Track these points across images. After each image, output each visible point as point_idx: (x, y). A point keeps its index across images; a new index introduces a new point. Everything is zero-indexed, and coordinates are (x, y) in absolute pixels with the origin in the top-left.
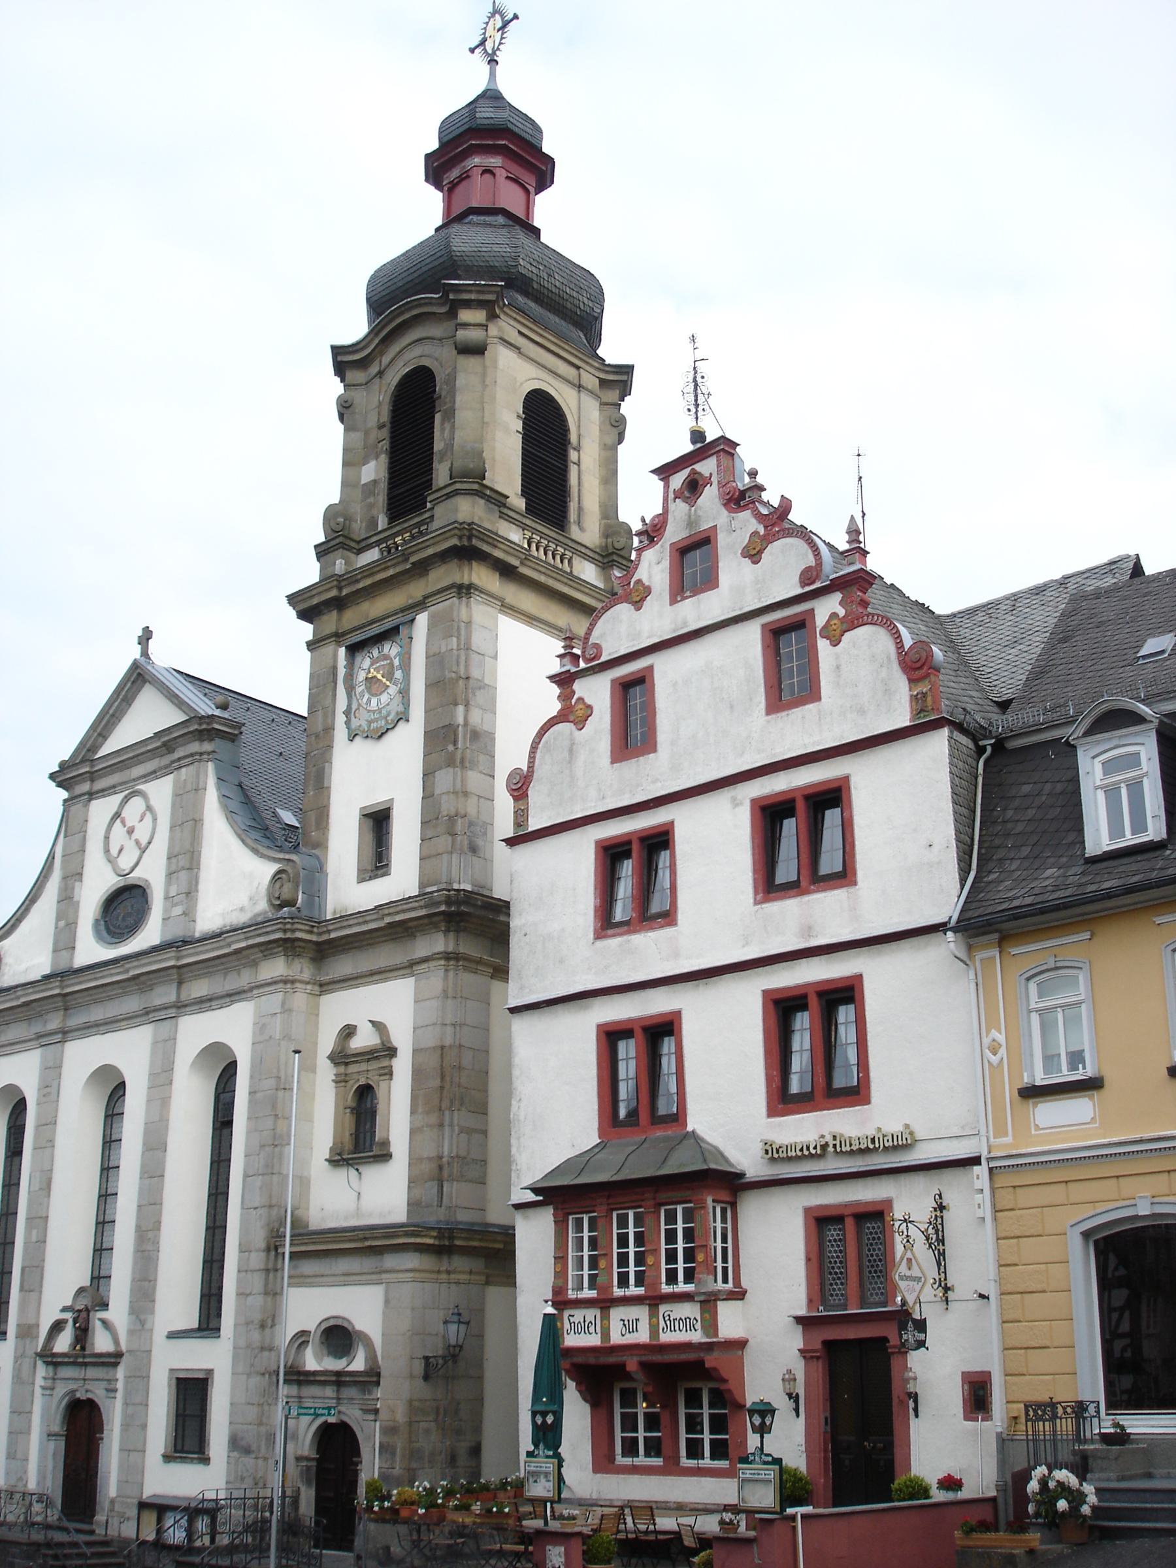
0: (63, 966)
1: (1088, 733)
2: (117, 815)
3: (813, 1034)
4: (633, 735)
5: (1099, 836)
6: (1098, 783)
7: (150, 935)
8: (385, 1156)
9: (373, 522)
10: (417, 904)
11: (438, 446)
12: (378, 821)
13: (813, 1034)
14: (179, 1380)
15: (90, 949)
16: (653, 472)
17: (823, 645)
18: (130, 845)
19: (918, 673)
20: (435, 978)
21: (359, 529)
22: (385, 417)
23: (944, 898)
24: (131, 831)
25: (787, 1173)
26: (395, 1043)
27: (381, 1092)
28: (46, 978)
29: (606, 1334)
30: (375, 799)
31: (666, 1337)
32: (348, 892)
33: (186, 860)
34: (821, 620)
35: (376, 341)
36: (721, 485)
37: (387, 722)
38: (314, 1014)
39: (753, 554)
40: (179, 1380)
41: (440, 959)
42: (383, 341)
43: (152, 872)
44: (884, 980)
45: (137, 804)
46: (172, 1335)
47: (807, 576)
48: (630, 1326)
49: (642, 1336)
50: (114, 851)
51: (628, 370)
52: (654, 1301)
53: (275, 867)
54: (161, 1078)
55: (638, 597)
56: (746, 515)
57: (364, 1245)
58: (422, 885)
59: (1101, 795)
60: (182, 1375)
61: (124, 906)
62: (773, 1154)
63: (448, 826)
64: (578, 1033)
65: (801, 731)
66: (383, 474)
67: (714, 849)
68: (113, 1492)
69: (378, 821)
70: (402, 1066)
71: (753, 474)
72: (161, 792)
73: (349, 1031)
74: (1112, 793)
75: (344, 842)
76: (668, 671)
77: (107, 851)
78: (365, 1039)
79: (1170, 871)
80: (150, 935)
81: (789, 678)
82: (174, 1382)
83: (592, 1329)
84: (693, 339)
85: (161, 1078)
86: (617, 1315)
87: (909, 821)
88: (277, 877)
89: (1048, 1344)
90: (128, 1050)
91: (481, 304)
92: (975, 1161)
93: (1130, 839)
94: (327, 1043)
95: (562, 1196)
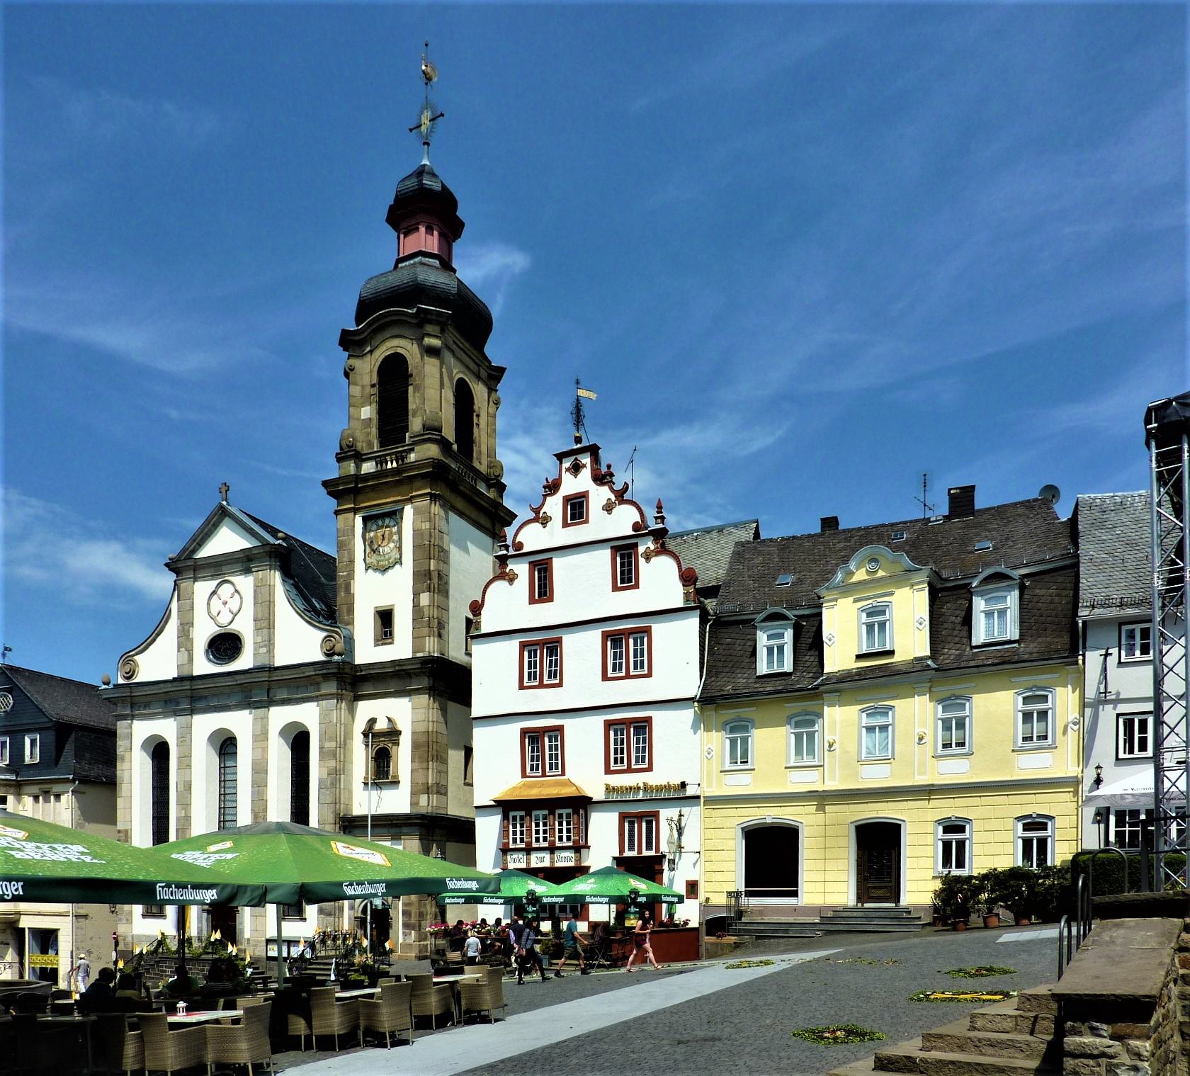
0: (185, 673)
1: (763, 621)
2: (214, 593)
3: (630, 734)
4: (542, 591)
5: (763, 668)
7: (245, 661)
8: (396, 783)
9: (370, 444)
11: (411, 406)
12: (385, 618)
13: (630, 734)
15: (203, 666)
17: (642, 561)
18: (225, 611)
20: (424, 699)
21: (361, 446)
22: (375, 380)
23: (691, 685)
24: (225, 603)
26: (399, 727)
27: (393, 753)
28: (175, 680)
29: (528, 863)
30: (384, 603)
31: (558, 865)
32: (367, 652)
33: (265, 622)
34: (641, 549)
36: (593, 470)
38: (352, 711)
39: (608, 508)
43: (244, 627)
44: (660, 718)
45: (226, 590)
47: (636, 527)
49: (547, 864)
50: (214, 613)
51: (501, 370)
52: (552, 849)
53: (325, 634)
54: (261, 737)
55: (545, 521)
56: (606, 488)
57: (390, 825)
58: (414, 652)
61: (225, 645)
62: (609, 789)
63: (431, 622)
64: (512, 731)
65: (628, 602)
66: (375, 417)
67: (582, 652)
68: (247, 934)
69: (385, 618)
70: (405, 742)
71: (609, 467)
72: (245, 583)
73: (372, 721)
74: (770, 650)
75: (363, 626)
76: (559, 565)
77: (209, 611)
78: (381, 725)
80: (245, 661)
81: (626, 577)
85: (261, 737)
86: (534, 856)
87: (678, 654)
88: (326, 639)
90: (239, 722)
91: (438, 323)
92: (698, 797)
93: (776, 670)
94: (359, 725)
95: (506, 807)
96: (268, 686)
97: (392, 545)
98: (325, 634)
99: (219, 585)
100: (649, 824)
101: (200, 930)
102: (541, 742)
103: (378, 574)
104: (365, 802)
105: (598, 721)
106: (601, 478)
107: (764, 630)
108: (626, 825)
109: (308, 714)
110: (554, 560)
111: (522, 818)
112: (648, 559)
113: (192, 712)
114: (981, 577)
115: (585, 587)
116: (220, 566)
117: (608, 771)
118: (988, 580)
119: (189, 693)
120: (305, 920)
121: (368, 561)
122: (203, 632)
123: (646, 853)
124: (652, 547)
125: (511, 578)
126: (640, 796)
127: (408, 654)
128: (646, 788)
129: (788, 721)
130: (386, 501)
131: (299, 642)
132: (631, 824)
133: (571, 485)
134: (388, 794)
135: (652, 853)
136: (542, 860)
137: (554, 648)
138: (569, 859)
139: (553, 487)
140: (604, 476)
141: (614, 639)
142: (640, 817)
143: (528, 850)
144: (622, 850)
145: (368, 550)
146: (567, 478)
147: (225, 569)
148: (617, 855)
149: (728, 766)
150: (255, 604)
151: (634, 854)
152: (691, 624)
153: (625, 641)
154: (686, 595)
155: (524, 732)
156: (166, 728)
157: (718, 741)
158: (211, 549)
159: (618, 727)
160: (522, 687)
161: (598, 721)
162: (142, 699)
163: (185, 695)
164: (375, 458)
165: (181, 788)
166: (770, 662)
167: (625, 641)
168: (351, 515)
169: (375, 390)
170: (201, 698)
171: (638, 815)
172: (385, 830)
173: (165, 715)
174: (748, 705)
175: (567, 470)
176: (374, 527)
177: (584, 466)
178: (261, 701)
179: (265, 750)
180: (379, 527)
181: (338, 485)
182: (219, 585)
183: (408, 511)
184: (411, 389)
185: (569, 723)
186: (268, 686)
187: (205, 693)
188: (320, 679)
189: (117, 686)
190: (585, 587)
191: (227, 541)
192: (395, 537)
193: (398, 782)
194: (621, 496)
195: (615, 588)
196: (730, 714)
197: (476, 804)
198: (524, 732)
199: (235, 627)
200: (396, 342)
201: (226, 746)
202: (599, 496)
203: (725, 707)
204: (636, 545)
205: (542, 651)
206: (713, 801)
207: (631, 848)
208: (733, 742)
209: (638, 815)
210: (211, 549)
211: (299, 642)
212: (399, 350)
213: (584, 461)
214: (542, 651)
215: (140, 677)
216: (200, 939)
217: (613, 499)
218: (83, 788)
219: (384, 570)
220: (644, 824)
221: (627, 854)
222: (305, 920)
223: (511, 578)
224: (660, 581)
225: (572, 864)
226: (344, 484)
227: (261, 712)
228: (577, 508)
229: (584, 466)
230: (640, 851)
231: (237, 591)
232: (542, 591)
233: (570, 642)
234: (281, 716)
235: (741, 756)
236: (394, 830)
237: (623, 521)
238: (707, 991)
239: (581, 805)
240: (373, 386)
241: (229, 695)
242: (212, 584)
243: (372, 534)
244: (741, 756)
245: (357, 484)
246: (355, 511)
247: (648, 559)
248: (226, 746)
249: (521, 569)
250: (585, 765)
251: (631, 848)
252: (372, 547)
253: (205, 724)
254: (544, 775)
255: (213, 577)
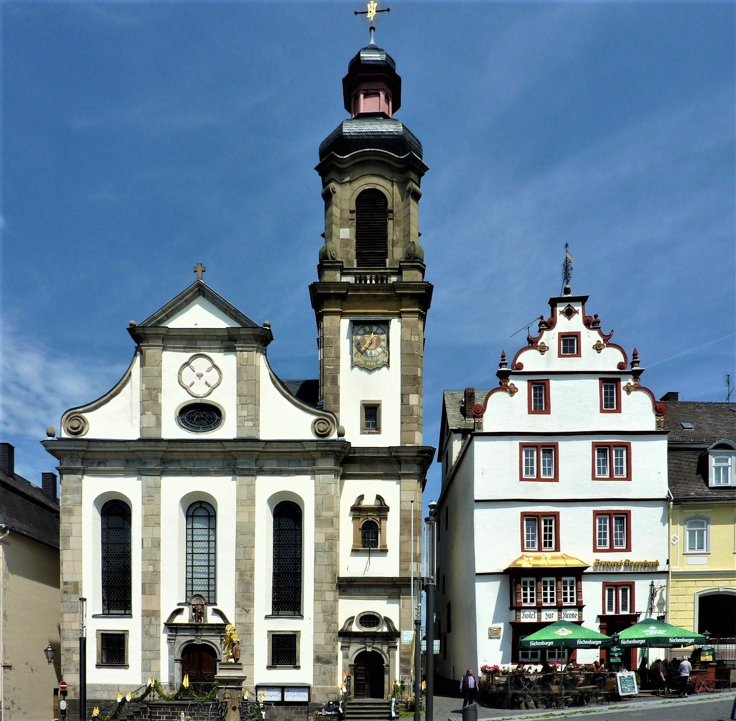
0: (152, 435)
2: (187, 364)
3: (614, 523)
4: (540, 402)
6: (713, 465)
7: (227, 430)
8: (384, 551)
10: (412, 450)
12: (371, 414)
13: (614, 523)
14: (273, 635)
15: (172, 430)
16: (588, 297)
17: (623, 393)
19: (660, 414)
23: (662, 490)
25: (602, 572)
29: (539, 618)
30: (372, 398)
33: (249, 398)
34: (623, 384)
35: (352, 163)
37: (377, 364)
39: (598, 348)
40: (102, 634)
41: (417, 475)
42: (354, 165)
43: (225, 398)
44: (638, 513)
45: (201, 364)
46: (94, 616)
47: (620, 366)
48: (551, 616)
52: (560, 608)
53: (315, 418)
54: (246, 502)
55: (543, 349)
58: (401, 443)
59: (714, 469)
60: (104, 632)
67: (576, 457)
72: (227, 362)
74: (718, 469)
76: (556, 386)
77: (220, 373)
78: (369, 501)
79: (735, 496)
82: (100, 636)
83: (533, 616)
84: (567, 246)
85: (246, 502)
87: (651, 466)
89: (684, 625)
90: (221, 489)
92: (667, 572)
93: (722, 484)
95: (514, 576)
96: (249, 457)
97: (379, 350)
98: (315, 418)
99: (193, 358)
100: (624, 591)
101: (172, 678)
102: (541, 526)
103: (364, 373)
104: (353, 566)
105: (516, 511)
106: (591, 323)
107: (714, 455)
108: (607, 592)
109: (302, 487)
110: (551, 381)
111: (532, 583)
112: (628, 391)
113: (163, 473)
114: (714, 444)
115: (575, 405)
116: (194, 340)
117: (595, 550)
118: (716, 448)
119: (160, 455)
120: (298, 667)
121: (355, 359)
122: (173, 399)
123: (622, 613)
124: (632, 383)
125: (512, 391)
126: (622, 570)
127: (396, 442)
128: (628, 564)
129: (683, 523)
130: (375, 312)
131: (285, 421)
132: (610, 591)
133: (563, 324)
134: (376, 560)
135: (627, 613)
136: (551, 616)
137: (551, 450)
138: (573, 616)
139: (550, 325)
140: (594, 324)
141: (601, 449)
142: (617, 586)
143: (539, 608)
144: (604, 611)
145: (355, 350)
146: (561, 319)
147: (200, 344)
148: (601, 614)
149: (687, 551)
150: (239, 380)
151: (613, 613)
152: (662, 445)
153: (611, 452)
154: (658, 423)
155: (524, 515)
156: (129, 487)
157: (680, 532)
158: (179, 322)
159: (548, 518)
160: (522, 479)
161: (588, 511)
162: (96, 456)
163: (149, 456)
164: (355, 274)
165: (148, 544)
166: (718, 479)
167: (611, 452)
168: (338, 318)
169: (354, 216)
170: (171, 461)
171: (618, 585)
172: (382, 590)
173: (126, 473)
174: (706, 507)
175: (562, 312)
176: (361, 332)
177: (576, 312)
178: (249, 470)
179: (252, 514)
180: (366, 333)
181: (329, 288)
182: (193, 358)
183: (395, 325)
184: (390, 223)
185: (564, 512)
186: (249, 457)
187: (176, 456)
188: (319, 455)
189: (61, 440)
190: (575, 405)
191: (198, 317)
192: (384, 344)
193: (387, 551)
194: (608, 341)
195: (602, 411)
196: (691, 513)
197: (477, 572)
198: (524, 515)
199: (213, 399)
200: (375, 180)
201: (200, 510)
202: (589, 338)
203: (690, 507)
204: (619, 380)
205: (541, 451)
206: (679, 575)
207: (610, 609)
208: (692, 534)
209: (618, 585)
210: (179, 322)
211: (285, 421)
212: (378, 188)
213: (576, 308)
214: (541, 451)
215: (89, 435)
216: (171, 685)
217: (602, 342)
218: (11, 540)
219: (370, 370)
220: (620, 592)
221: (608, 613)
222: (298, 667)
223: (512, 391)
224: (637, 411)
225: (535, 620)
226: (335, 289)
227: (247, 479)
228: (570, 344)
229: (576, 312)
230: (617, 611)
231: (215, 367)
232: (540, 402)
233: (565, 447)
234: (268, 486)
235: (698, 543)
236: (395, 590)
237: (610, 360)
238: (433, 687)
239: (578, 573)
240: (352, 212)
241: (208, 461)
242: (186, 356)
243: (359, 337)
244: (698, 543)
245: (348, 291)
246: (343, 315)
247: (628, 391)
248: (200, 510)
249: (521, 385)
250: (577, 544)
251: (610, 609)
252: (358, 348)
253: (176, 488)
254: (540, 550)
255: (186, 349)
